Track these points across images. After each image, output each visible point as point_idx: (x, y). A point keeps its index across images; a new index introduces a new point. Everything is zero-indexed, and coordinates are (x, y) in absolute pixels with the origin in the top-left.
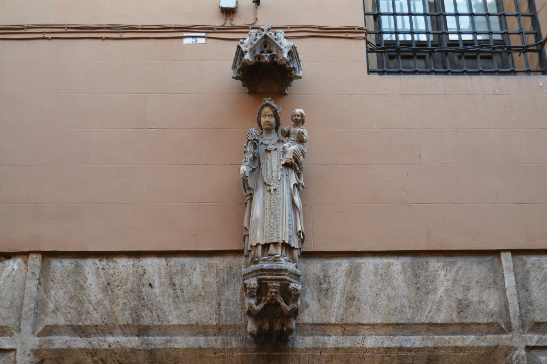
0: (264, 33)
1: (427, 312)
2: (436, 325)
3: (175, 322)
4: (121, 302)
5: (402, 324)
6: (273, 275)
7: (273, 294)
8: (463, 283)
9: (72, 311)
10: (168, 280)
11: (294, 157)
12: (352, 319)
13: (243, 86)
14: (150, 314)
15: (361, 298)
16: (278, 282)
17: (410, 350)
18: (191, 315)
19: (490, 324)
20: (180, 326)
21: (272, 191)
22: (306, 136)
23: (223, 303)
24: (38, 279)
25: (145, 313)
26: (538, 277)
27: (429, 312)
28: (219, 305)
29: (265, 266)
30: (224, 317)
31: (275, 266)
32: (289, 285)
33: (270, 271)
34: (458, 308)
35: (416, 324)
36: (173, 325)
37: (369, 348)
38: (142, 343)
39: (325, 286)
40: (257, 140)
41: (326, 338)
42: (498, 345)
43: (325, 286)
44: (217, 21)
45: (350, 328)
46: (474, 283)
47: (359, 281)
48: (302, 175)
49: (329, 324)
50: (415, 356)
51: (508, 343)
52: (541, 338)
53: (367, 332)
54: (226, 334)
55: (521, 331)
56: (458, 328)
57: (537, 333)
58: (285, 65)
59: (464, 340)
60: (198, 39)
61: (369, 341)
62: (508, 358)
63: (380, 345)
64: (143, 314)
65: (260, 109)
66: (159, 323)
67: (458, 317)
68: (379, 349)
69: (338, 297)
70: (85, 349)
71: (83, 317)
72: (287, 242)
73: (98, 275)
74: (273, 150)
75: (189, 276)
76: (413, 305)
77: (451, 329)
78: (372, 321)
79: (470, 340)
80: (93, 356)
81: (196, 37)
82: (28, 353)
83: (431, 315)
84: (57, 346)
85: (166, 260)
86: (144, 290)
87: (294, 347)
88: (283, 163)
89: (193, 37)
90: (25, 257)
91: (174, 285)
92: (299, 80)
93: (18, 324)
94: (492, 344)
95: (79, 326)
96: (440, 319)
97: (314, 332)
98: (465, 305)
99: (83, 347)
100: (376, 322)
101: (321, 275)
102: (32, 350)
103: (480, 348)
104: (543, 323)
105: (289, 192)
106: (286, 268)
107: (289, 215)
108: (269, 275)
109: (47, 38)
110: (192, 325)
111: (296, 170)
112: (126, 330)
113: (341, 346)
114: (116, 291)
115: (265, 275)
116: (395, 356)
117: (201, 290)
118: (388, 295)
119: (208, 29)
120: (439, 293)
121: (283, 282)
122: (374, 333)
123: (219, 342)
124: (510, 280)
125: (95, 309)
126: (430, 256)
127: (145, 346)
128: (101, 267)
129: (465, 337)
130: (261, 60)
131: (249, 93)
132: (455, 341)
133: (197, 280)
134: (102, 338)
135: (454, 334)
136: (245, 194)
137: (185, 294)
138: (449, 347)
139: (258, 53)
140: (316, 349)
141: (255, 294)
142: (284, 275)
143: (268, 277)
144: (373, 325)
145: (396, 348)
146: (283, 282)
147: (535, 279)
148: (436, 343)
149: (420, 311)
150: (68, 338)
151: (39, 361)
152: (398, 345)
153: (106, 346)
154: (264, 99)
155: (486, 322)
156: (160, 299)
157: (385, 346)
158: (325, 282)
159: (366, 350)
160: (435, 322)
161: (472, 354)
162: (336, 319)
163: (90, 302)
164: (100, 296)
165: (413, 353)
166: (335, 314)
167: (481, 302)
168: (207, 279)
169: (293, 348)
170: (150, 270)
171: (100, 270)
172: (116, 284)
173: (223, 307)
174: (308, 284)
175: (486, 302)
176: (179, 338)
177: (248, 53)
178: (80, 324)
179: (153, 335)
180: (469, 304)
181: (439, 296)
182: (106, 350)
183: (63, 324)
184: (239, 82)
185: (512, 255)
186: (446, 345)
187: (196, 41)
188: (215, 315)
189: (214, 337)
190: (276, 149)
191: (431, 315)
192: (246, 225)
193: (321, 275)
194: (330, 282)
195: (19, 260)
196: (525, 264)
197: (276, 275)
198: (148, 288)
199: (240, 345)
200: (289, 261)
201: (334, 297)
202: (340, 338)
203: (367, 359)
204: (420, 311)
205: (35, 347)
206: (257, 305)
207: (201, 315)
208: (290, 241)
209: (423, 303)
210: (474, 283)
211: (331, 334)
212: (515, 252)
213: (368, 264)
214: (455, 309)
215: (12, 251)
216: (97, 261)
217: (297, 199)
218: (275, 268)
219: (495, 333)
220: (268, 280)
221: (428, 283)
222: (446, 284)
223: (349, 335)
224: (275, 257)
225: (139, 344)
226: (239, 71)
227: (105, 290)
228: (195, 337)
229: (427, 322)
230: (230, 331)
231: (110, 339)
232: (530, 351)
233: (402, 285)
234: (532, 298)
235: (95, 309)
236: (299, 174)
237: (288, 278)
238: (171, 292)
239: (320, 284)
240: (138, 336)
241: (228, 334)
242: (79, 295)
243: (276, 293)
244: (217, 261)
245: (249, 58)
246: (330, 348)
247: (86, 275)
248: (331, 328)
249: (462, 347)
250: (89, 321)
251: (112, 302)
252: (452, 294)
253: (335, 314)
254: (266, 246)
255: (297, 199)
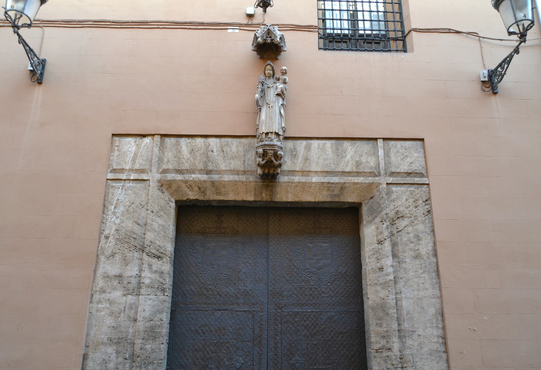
0: (268, 27)
1: (341, 166)
2: (345, 172)
3: (224, 168)
4: (198, 159)
5: (330, 172)
6: (270, 147)
7: (270, 156)
8: (359, 153)
9: (175, 162)
10: (220, 149)
11: (281, 91)
12: (306, 169)
13: (257, 54)
14: (212, 165)
15: (311, 159)
16: (273, 151)
17: (333, 183)
18: (231, 165)
19: (371, 173)
20: (226, 170)
21: (270, 107)
22: (287, 80)
23: (246, 160)
24: (159, 147)
25: (210, 164)
26: (395, 151)
27: (343, 166)
28: (244, 161)
29: (267, 143)
30: (247, 167)
31: (271, 143)
32: (277, 152)
33: (269, 145)
34: (356, 165)
35: (336, 172)
36: (223, 170)
37: (314, 182)
38: (208, 178)
39: (294, 153)
40: (263, 82)
41: (294, 177)
42: (374, 182)
43: (294, 153)
44: (245, 21)
45: (306, 173)
46: (364, 153)
47: (310, 151)
48: (285, 100)
49: (296, 171)
50: (335, 186)
51: (378, 181)
52: (394, 180)
53: (313, 175)
54: (248, 174)
55: (385, 176)
56: (356, 174)
57: (392, 177)
58: (278, 44)
59: (358, 179)
60: (235, 30)
61: (314, 179)
62: (378, 188)
63: (319, 181)
64: (209, 165)
65: (265, 66)
66: (217, 169)
67: (356, 169)
68: (318, 183)
69: (300, 159)
70: (182, 180)
71: (181, 165)
72: (277, 132)
73: (187, 146)
74: (271, 87)
75: (230, 147)
76: (335, 163)
77: (352, 174)
78: (316, 170)
79: (361, 179)
80: (185, 183)
81: (234, 29)
82: (155, 181)
83: (343, 167)
84: (169, 179)
85: (220, 139)
86: (209, 153)
87: (279, 181)
88: (276, 93)
89: (233, 29)
90: (153, 136)
91: (223, 151)
92: (285, 52)
93: (150, 168)
94: (371, 182)
95: (179, 170)
96: (348, 169)
97: (289, 174)
98: (360, 163)
99: (181, 179)
100: (318, 171)
101: (293, 148)
102: (157, 180)
103: (365, 183)
104: (395, 172)
105: (278, 108)
106: (276, 144)
107: (278, 119)
108: (269, 147)
109: (160, 28)
110: (231, 170)
111: (282, 97)
112: (201, 171)
113: (301, 181)
114: (196, 153)
115: (266, 147)
116: (326, 186)
117: (236, 154)
118: (324, 158)
119: (240, 25)
120: (348, 157)
121: (275, 151)
122: (316, 175)
123: (244, 178)
124: (381, 152)
125: (186, 162)
126: (345, 140)
127: (210, 179)
128: (189, 142)
129: (358, 178)
130: (266, 42)
131: (260, 58)
132: (354, 180)
133: (234, 149)
134: (189, 175)
135: (353, 176)
136: (257, 109)
137: (229, 156)
138: (351, 183)
139: (265, 38)
140: (289, 182)
141: (261, 156)
142: (275, 147)
143: (268, 148)
144: (316, 172)
145: (326, 182)
146: (275, 151)
147: (393, 152)
148: (345, 181)
149: (338, 166)
150: (174, 175)
151: (161, 185)
152: (327, 181)
153: (192, 179)
154: (267, 61)
155: (369, 171)
156: (217, 158)
157: (321, 182)
158: (294, 151)
159: (312, 183)
160: (345, 171)
161: (362, 186)
162: (299, 169)
163: (184, 158)
164: (189, 156)
165: (334, 185)
166: (299, 166)
167: (367, 162)
168: (239, 149)
169: (278, 182)
170: (212, 144)
171: (188, 143)
172: (196, 150)
173: (246, 162)
174: (287, 152)
175: (370, 162)
176: (226, 176)
177: (260, 38)
178: (179, 168)
179: (213, 174)
180: (362, 163)
181: (347, 159)
182: (192, 181)
183: (171, 168)
184: (255, 52)
185: (383, 141)
186: (350, 182)
187: (234, 31)
188: (242, 166)
189: (242, 176)
190: (273, 87)
191: (343, 167)
192: (257, 123)
193: (293, 148)
194: (297, 151)
195: (150, 138)
196: (389, 145)
197: (272, 147)
198: (211, 152)
199: (254, 180)
200: (278, 141)
201: (298, 158)
202: (301, 178)
203: (313, 187)
204: (338, 166)
205: (159, 179)
206: (262, 161)
207: (236, 165)
208: (278, 131)
209: (340, 162)
210: (364, 153)
211: (296, 175)
212: (384, 139)
213: (315, 143)
214: (355, 165)
215: (146, 133)
216: (187, 139)
217: (282, 111)
218: (271, 144)
219: (373, 177)
220: (268, 150)
221: (343, 153)
222: (351, 153)
223: (305, 176)
224: (271, 139)
225: (207, 178)
226: (255, 46)
227: (191, 153)
228: (233, 176)
229: (341, 171)
230: (249, 173)
231: (193, 176)
232: (388, 185)
233: (331, 153)
234: (391, 161)
235: (186, 162)
236: (283, 99)
237: (277, 149)
238: (222, 154)
239: (292, 152)
240: (206, 175)
241: (249, 174)
242: (178, 155)
243: (271, 156)
244: (243, 140)
245: (260, 40)
246: (296, 182)
247: (182, 146)
248: (297, 173)
249: (357, 183)
250: (183, 167)
251: (194, 159)
252: (354, 158)
253: (299, 166)
254: (267, 134)
255: (282, 111)
